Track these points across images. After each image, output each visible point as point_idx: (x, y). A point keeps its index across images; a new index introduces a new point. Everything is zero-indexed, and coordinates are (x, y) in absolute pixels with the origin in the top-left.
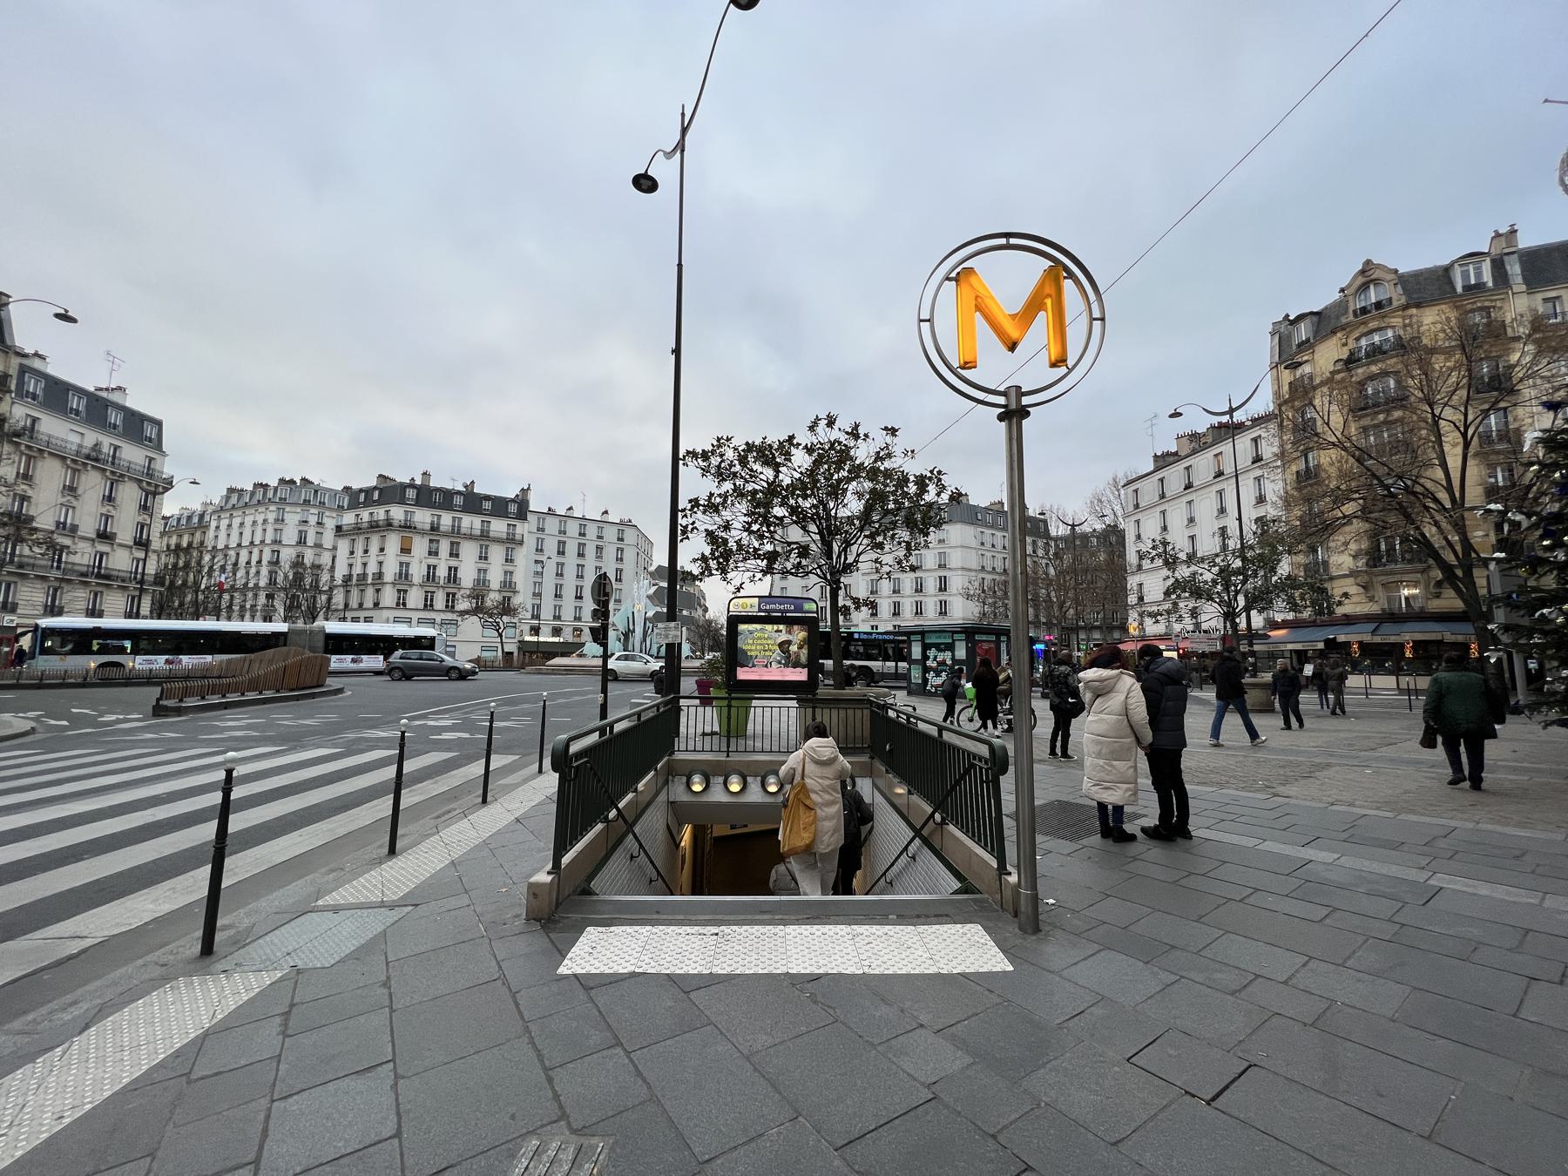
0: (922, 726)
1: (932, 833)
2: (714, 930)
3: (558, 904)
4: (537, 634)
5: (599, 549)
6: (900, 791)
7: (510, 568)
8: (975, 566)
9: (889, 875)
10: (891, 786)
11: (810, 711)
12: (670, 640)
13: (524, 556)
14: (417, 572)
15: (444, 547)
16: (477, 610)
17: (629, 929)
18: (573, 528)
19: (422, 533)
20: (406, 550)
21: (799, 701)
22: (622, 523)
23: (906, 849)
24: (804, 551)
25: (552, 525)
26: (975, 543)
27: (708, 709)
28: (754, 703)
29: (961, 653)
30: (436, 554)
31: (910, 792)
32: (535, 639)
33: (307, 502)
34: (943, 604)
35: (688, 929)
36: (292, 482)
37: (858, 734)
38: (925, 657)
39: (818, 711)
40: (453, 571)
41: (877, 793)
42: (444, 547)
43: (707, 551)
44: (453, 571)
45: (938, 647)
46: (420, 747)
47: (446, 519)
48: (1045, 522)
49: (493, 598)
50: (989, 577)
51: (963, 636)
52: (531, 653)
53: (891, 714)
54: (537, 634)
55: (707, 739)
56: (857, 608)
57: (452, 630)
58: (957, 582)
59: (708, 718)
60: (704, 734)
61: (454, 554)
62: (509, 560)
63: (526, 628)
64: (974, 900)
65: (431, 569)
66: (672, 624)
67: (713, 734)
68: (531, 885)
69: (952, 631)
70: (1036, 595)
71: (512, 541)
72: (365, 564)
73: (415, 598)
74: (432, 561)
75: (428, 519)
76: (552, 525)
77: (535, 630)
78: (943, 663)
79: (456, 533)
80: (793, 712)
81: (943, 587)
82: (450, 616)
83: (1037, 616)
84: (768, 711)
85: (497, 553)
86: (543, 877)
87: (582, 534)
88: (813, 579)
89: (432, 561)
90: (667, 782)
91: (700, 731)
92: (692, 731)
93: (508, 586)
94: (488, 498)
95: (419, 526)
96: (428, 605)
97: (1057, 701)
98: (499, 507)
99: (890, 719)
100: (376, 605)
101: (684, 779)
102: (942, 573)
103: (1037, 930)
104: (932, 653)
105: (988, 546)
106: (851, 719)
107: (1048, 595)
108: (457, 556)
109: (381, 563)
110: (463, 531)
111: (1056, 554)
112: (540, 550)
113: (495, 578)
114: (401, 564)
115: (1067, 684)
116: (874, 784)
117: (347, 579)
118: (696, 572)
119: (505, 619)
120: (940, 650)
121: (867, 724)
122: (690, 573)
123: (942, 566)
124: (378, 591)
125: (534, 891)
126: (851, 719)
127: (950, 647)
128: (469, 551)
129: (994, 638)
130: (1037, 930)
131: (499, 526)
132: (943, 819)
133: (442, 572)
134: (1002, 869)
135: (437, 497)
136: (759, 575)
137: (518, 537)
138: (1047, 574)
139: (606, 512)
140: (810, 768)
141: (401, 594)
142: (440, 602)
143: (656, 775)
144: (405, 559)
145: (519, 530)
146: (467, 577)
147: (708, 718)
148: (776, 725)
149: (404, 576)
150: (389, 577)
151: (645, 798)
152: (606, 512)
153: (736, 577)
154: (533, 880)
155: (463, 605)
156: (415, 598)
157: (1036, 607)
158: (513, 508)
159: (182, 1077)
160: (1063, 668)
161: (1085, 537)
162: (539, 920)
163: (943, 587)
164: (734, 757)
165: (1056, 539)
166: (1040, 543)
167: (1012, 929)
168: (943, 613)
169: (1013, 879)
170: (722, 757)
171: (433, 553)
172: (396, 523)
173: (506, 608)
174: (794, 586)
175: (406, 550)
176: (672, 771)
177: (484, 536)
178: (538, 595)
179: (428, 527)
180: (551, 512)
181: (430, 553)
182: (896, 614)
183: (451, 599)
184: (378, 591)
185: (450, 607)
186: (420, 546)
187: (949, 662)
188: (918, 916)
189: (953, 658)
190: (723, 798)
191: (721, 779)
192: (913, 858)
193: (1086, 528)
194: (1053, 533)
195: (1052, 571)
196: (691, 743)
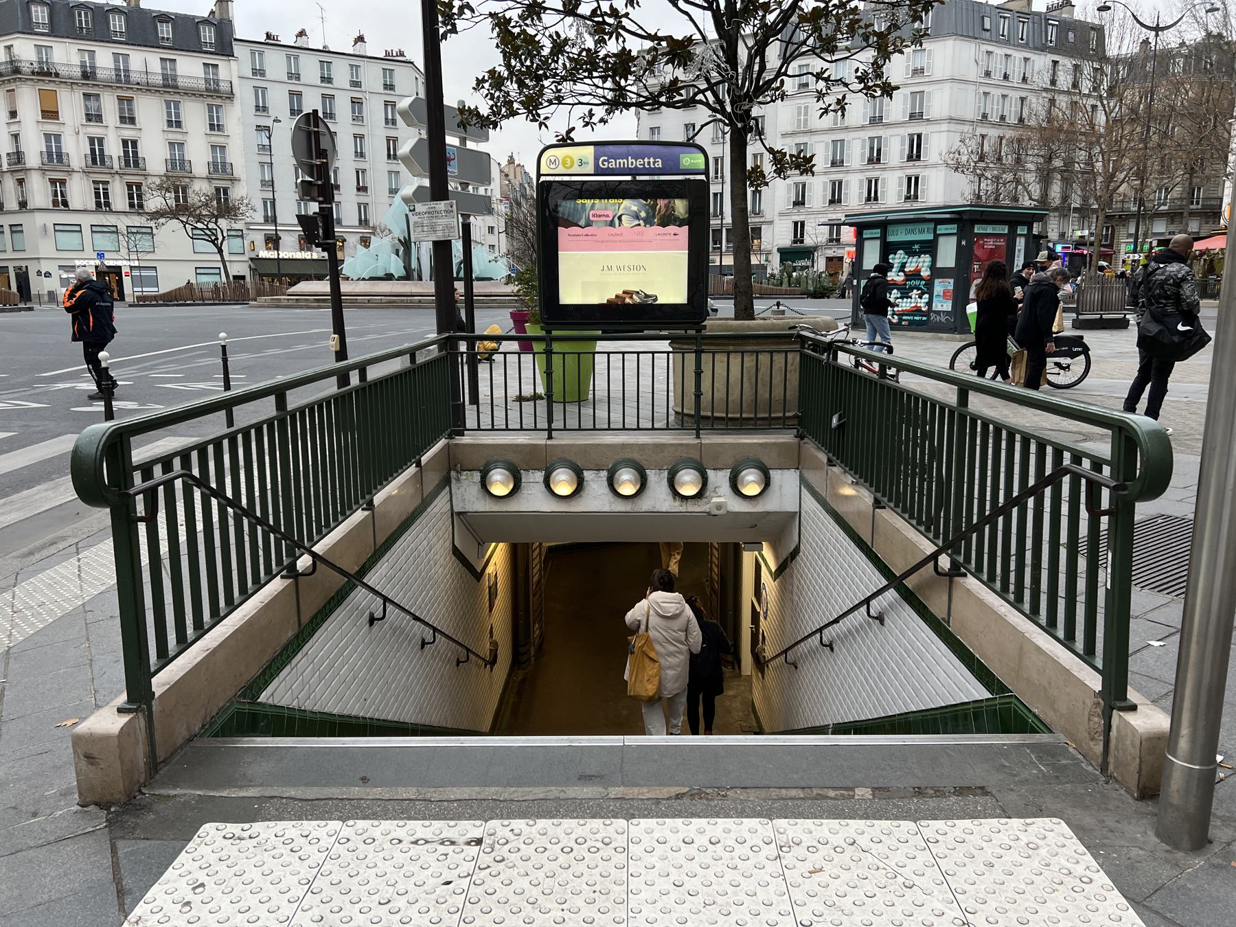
0: (908, 381)
1: (926, 585)
2: (472, 828)
3: (154, 765)
4: (277, 248)
5: (356, 103)
6: (848, 491)
7: (220, 140)
8: (971, 114)
9: (828, 634)
10: (834, 484)
11: (690, 358)
12: (439, 236)
13: (238, 117)
14: (76, 150)
15: (109, 105)
16: (181, 210)
17: (290, 828)
18: (310, 69)
19: (71, 83)
20: (50, 114)
21: (674, 340)
22: (389, 57)
23: (867, 601)
24: (679, 51)
25: (275, 63)
26: (974, 73)
27: (527, 359)
28: (601, 346)
29: (947, 254)
30: (99, 118)
31: (877, 504)
32: (272, 254)
34: (913, 183)
35: (419, 828)
37: (778, 393)
38: (884, 267)
39: (706, 358)
40: (130, 146)
41: (806, 494)
42: (109, 105)
43: (496, 60)
44: (130, 146)
45: (909, 248)
46: (52, 425)
47: (104, 58)
48: (1099, 30)
49: (200, 190)
50: (993, 133)
51: (953, 228)
52: (273, 276)
53: (845, 360)
54: (277, 248)
55: (528, 407)
56: (780, 172)
57: (144, 243)
58: (938, 144)
59: (527, 373)
60: (520, 399)
61: (128, 119)
62: (216, 127)
63: (259, 238)
64: (1034, 747)
65: (96, 144)
66: (441, 205)
67: (535, 397)
68: (78, 740)
69: (936, 219)
70: (1069, 163)
71: (215, 95)
73: (80, 192)
74: (95, 131)
75: (75, 59)
76: (275, 63)
77: (273, 241)
78: (916, 275)
79: (122, 80)
80: (661, 360)
81: (915, 152)
82: (137, 221)
83: (1065, 198)
84: (631, 360)
85: (194, 115)
86: (108, 721)
87: (327, 79)
88: (701, 114)
89: (95, 131)
90: (446, 482)
91: (513, 392)
92: (499, 393)
93: (220, 169)
94: (164, 17)
95: (63, 71)
96: (102, 203)
97: (1154, 328)
98: (185, 33)
99: (842, 370)
100: (23, 204)
101: (477, 476)
102: (915, 129)
103: (1200, 841)
104: (897, 258)
105: (997, 76)
106: (764, 370)
107: (1090, 162)
108: (132, 120)
110: (134, 77)
111: (1111, 91)
112: (261, 109)
113: (198, 156)
114: (47, 137)
115: (1177, 298)
116: (803, 482)
118: (485, 110)
119: (223, 223)
120: (911, 253)
121: (794, 378)
122: (475, 113)
123: (916, 117)
124: (21, 182)
125: (89, 750)
126: (764, 370)
127: (930, 248)
128: (150, 111)
129: (1004, 230)
130: (1200, 841)
131: (190, 68)
132: (955, 565)
133: (114, 149)
134: (1115, 695)
136: (600, 112)
137: (224, 87)
138: (1092, 125)
139: (360, 39)
140: (654, 620)
141: (58, 184)
142: (119, 199)
143: (419, 478)
144: (52, 128)
145: (223, 73)
146: (155, 155)
147: (527, 373)
148: (646, 382)
149: (55, 156)
150: (33, 159)
151: (397, 515)
152: (360, 39)
153: (559, 119)
154: (84, 728)
155: (154, 202)
156: (80, 192)
157: (1067, 182)
158: (208, 35)
160: (1173, 268)
161: (1166, 56)
162: (103, 805)
163: (915, 152)
164: (562, 439)
165: (1117, 61)
166: (1087, 69)
167: (1140, 835)
168: (912, 196)
169: (1149, 719)
170: (540, 439)
171: (94, 117)
172: (26, 68)
173: (224, 206)
174: (671, 124)
175: (50, 114)
176: (452, 466)
177: (169, 86)
178: (270, 184)
179: (77, 72)
180: (271, 40)
181: (89, 117)
182: (835, 200)
183: (135, 194)
184: (21, 182)
185: (136, 205)
186: (71, 104)
187: (925, 273)
188: (919, 792)
189: (933, 267)
190: (545, 505)
191: (539, 476)
192: (880, 619)
193: (1170, 39)
194: (1112, 50)
195: (1101, 118)
196: (499, 414)
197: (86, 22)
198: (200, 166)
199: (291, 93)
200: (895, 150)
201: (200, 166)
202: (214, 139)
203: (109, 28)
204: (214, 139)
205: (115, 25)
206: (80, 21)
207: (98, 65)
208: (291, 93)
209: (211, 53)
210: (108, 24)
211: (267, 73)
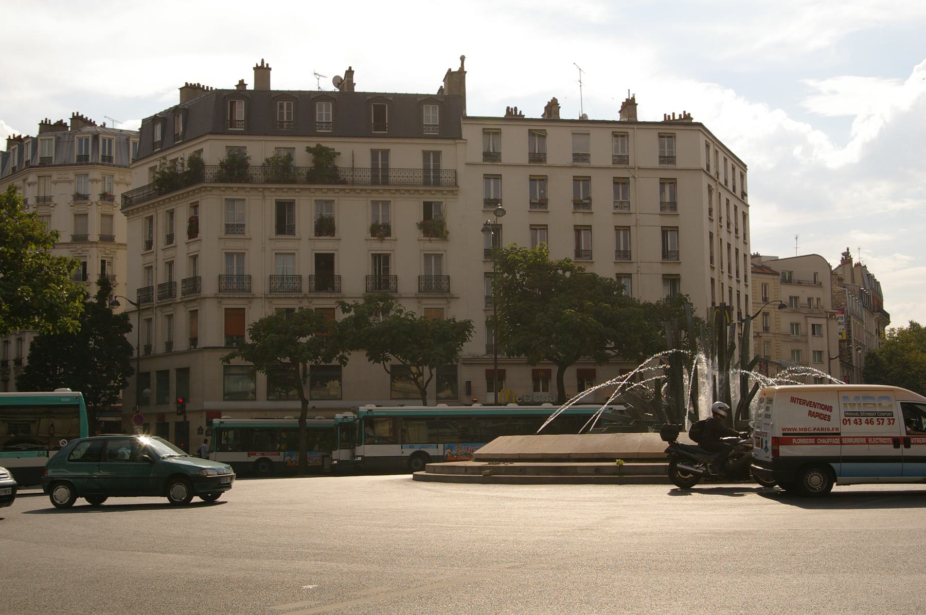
5: (621, 184)
33: (83, 160)
36: (60, 124)
72: (170, 264)
109: (194, 258)
114: (229, 255)
117: (145, 295)
131: (406, 157)
135: (285, 112)
144: (235, 245)
150: (209, 287)
158: (431, 116)
159: (113, 422)
197: (289, 114)
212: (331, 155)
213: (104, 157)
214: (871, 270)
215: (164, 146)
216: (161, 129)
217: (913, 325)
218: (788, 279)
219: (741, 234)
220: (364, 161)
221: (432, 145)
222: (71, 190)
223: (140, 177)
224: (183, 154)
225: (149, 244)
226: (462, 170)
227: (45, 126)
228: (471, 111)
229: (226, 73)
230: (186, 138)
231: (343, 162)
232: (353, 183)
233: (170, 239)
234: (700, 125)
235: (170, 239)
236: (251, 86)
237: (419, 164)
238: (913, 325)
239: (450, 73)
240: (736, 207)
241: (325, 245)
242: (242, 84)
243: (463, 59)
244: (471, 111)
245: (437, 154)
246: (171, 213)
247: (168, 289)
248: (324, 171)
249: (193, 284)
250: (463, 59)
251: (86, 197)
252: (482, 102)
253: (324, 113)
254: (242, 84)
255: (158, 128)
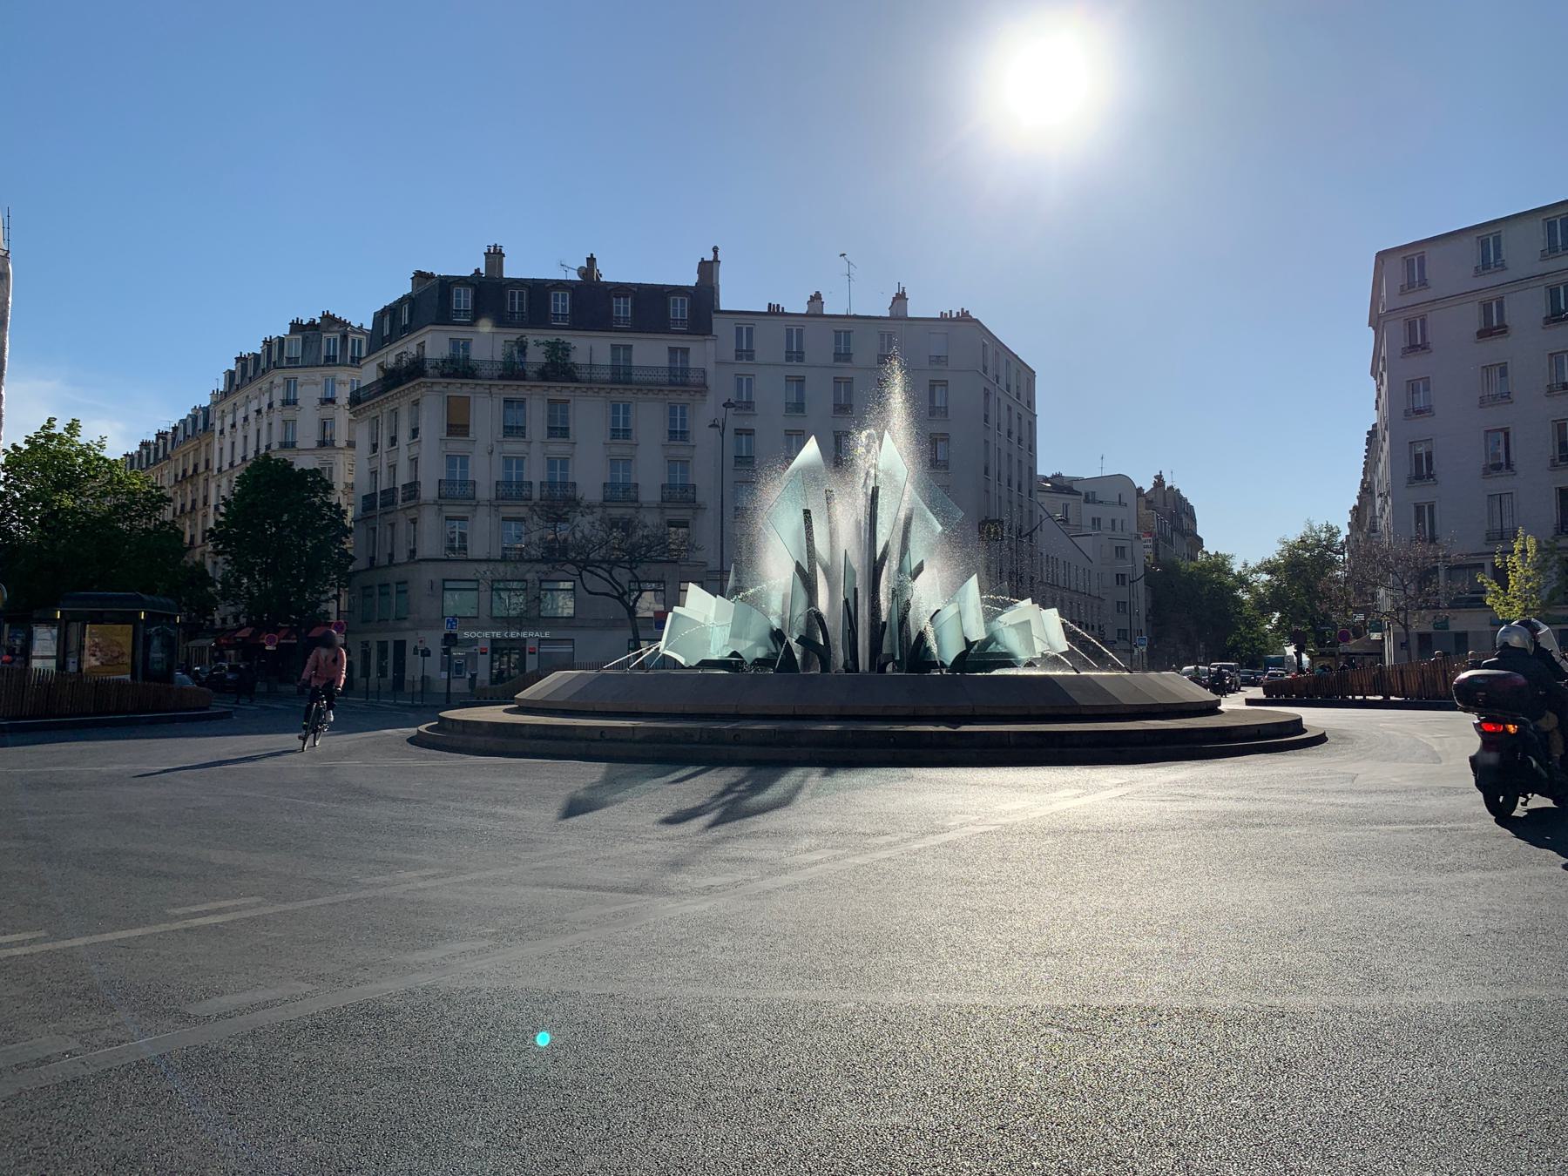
62: (678, 434)
74: (514, 447)
108: (565, 432)
113: (650, 476)
117: (369, 501)
131: (650, 352)
144: (457, 445)
145: (694, 362)
150: (428, 491)
171: (514, 431)
197: (521, 305)
198: (650, 493)
199: (837, 381)
200: (384, 442)
201: (650, 493)
202: (615, 450)
203: (450, 305)
204: (615, 450)
205: (556, 306)
206: (513, 304)
207: (635, 363)
208: (837, 381)
209: (682, 333)
210: (573, 305)
211: (757, 355)
212: (566, 349)
213: (353, 358)
214: (1183, 494)
215: (391, 339)
216: (393, 322)
217: (420, 277)
218: (1090, 499)
219: (1025, 442)
220: (604, 357)
221: (678, 342)
222: (318, 392)
223: (369, 374)
224: (408, 347)
225: (375, 447)
226: (711, 368)
227: (296, 327)
228: (724, 305)
229: (460, 260)
230: (409, 329)
231: (578, 357)
232: (590, 381)
233: (393, 440)
234: (977, 321)
235: (393, 440)
236: (483, 271)
237: (664, 361)
238: (420, 277)
239: (703, 263)
240: (1009, 409)
241: (558, 448)
242: (477, 271)
243: (715, 250)
244: (724, 305)
245: (686, 351)
246: (395, 412)
247: (390, 494)
248: (559, 369)
249: (412, 489)
250: (715, 250)
251: (332, 401)
252: (733, 296)
253: (561, 304)
254: (477, 271)
255: (387, 319)
